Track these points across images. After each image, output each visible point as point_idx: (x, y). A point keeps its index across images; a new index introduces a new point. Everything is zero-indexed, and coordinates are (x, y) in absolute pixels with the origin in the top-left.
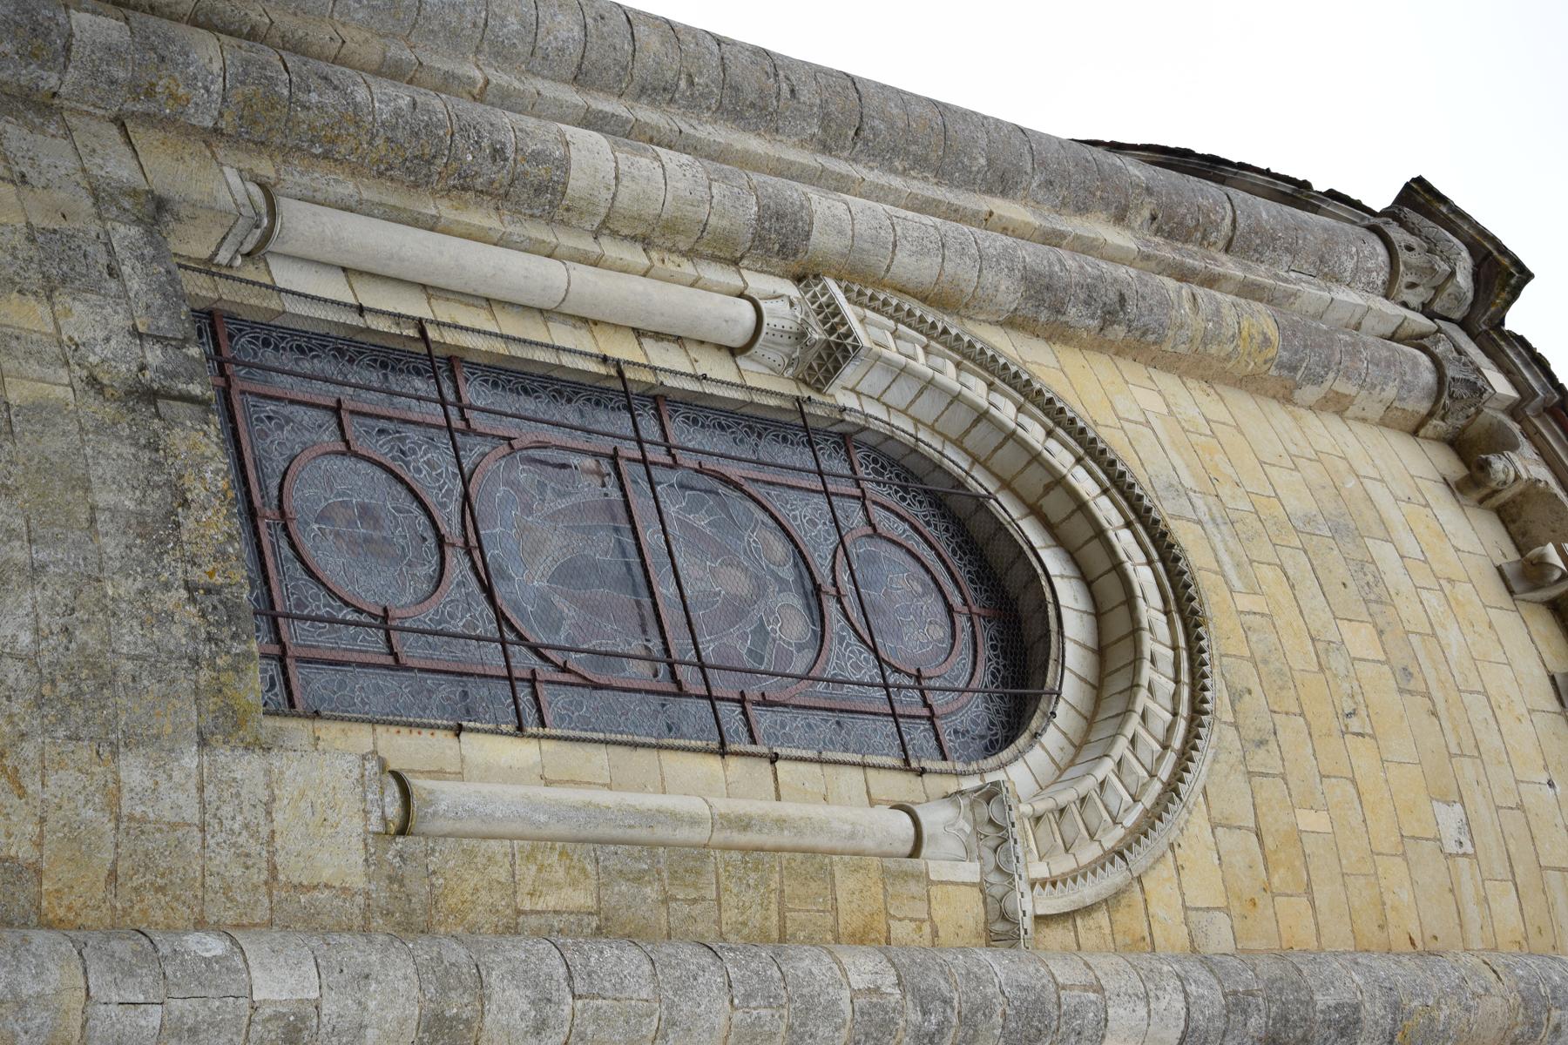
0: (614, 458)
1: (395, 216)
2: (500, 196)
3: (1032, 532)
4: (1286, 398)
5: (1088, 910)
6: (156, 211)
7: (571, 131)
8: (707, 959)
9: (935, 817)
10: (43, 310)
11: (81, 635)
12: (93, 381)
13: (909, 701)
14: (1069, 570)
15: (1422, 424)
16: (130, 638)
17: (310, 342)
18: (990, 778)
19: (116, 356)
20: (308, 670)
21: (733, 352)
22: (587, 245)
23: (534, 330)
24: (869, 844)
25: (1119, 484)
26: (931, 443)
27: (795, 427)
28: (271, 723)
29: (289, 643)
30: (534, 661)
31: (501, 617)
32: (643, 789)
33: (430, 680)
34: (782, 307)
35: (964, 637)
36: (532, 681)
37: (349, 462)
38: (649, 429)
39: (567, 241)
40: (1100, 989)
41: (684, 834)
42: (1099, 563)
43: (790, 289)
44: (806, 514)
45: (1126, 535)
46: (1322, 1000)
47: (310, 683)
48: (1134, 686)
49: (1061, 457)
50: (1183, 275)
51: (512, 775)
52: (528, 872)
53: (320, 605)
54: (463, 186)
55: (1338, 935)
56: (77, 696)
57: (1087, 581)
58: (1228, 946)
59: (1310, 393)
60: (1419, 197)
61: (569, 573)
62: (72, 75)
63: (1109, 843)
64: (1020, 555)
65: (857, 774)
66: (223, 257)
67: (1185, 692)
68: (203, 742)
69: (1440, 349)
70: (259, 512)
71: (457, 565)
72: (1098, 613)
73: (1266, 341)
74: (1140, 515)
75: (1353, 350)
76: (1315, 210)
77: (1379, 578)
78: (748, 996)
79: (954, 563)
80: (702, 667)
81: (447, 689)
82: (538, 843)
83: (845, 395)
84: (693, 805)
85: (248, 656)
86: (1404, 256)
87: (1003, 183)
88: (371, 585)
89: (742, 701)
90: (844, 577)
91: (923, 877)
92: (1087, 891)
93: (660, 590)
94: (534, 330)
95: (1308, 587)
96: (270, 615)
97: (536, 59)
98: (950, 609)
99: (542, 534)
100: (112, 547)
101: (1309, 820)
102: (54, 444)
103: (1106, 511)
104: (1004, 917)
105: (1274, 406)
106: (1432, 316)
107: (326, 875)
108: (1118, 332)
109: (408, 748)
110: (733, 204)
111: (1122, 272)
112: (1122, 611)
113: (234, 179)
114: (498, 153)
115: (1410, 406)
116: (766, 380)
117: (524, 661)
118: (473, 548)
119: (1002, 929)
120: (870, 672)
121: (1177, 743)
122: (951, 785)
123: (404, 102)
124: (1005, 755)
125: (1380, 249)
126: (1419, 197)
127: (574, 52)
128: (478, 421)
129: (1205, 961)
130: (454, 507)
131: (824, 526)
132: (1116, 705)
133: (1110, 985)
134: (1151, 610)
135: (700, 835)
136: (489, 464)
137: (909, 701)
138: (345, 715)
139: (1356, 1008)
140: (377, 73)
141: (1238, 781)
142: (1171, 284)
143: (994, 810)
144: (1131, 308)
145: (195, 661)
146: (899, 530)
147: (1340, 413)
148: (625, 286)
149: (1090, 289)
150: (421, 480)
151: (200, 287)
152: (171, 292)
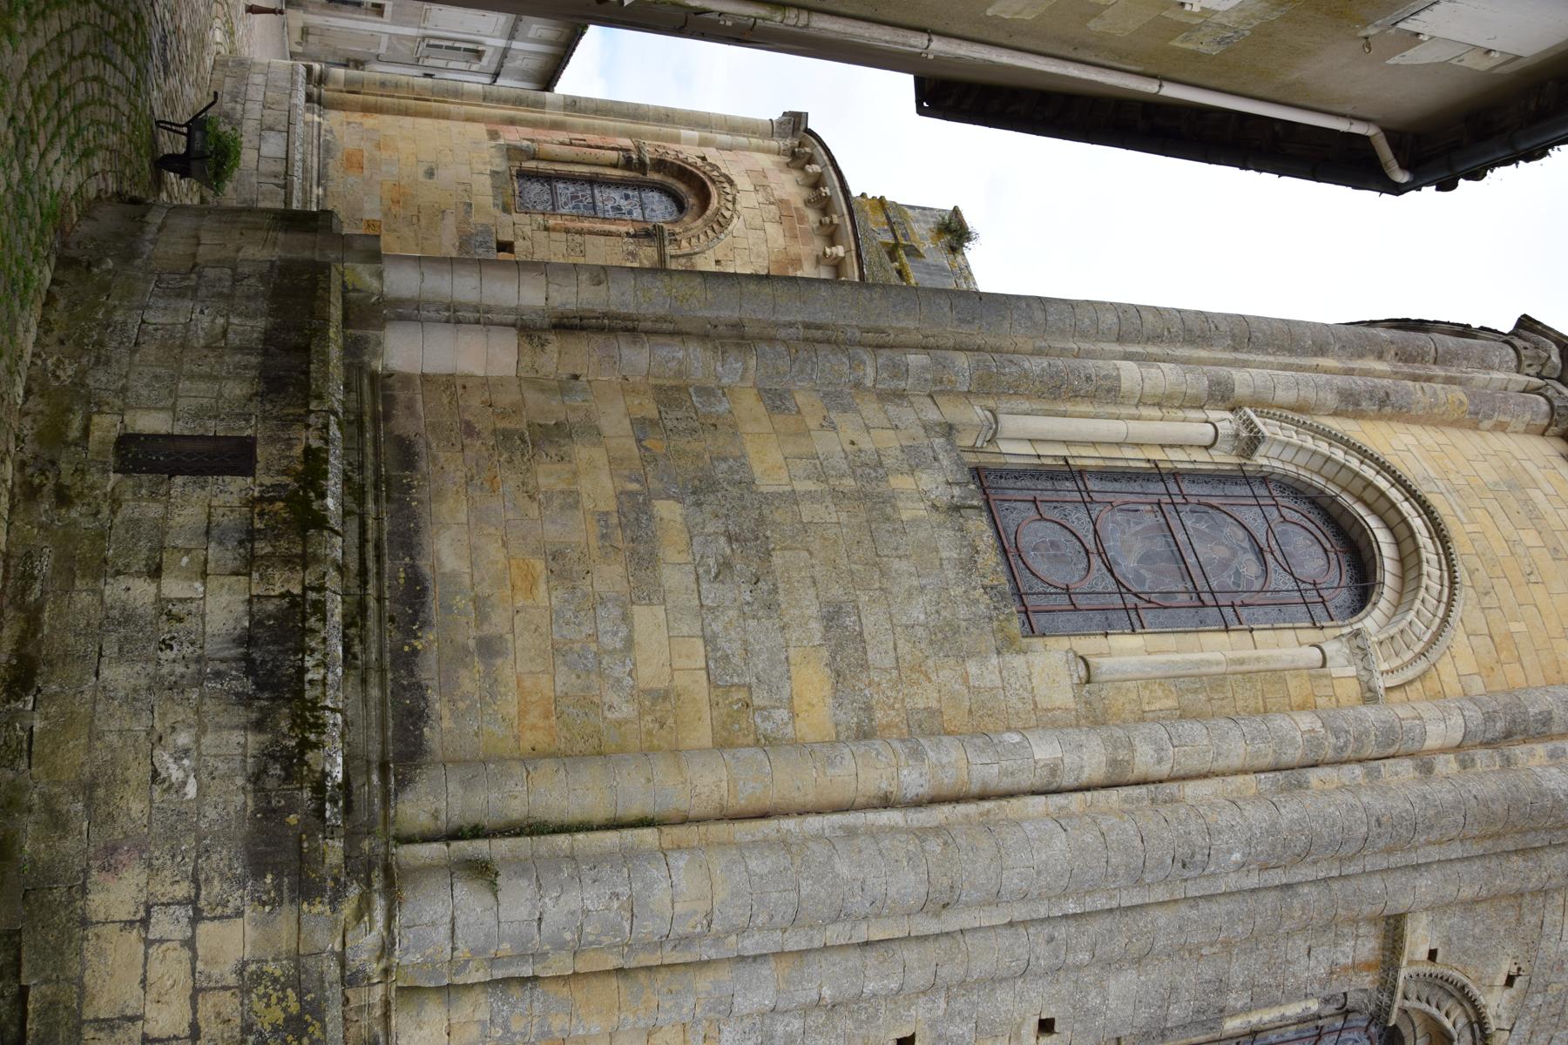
0: (1159, 504)
1: (1048, 413)
2: (1091, 397)
3: (1360, 509)
4: (1475, 427)
5: (1410, 682)
6: (949, 430)
7: (1118, 363)
8: (1232, 724)
9: (1331, 648)
10: (911, 480)
11: (944, 613)
12: (934, 506)
13: (1312, 596)
14: (1381, 525)
15: (1546, 430)
16: (963, 612)
17: (1019, 474)
18: (1356, 627)
19: (942, 494)
20: (1040, 616)
21: (1207, 448)
22: (1133, 411)
23: (1116, 453)
24: (1301, 664)
25: (1399, 481)
26: (1305, 475)
27: (1241, 477)
28: (1025, 641)
29: (1030, 607)
30: (1136, 600)
31: (1118, 582)
32: (1192, 651)
33: (1091, 614)
34: (1226, 424)
35: (1334, 562)
36: (1136, 609)
37: (1043, 523)
38: (1173, 488)
39: (1124, 411)
40: (1421, 718)
41: (1214, 669)
42: (1395, 519)
43: (1229, 415)
44: (1251, 516)
45: (1406, 504)
46: (1532, 711)
47: (1039, 621)
48: (1420, 575)
49: (1369, 472)
50: (1415, 378)
51: (1133, 652)
52: (1146, 694)
53: (1039, 587)
54: (1076, 395)
55: (1537, 678)
56: (945, 638)
57: (1390, 529)
58: (1483, 691)
59: (1487, 424)
60: (1526, 324)
61: (1146, 558)
62: (910, 381)
63: (1417, 649)
64: (1356, 521)
65: (1291, 633)
66: (979, 444)
67: (1446, 575)
68: (999, 653)
69: (1549, 394)
70: (1008, 550)
71: (1096, 561)
72: (1398, 543)
73: (1461, 403)
74: (1412, 494)
75: (1505, 400)
76: (1475, 337)
77: (1535, 507)
78: (1253, 739)
79: (1324, 529)
80: (1212, 593)
81: (1098, 616)
82: (1148, 681)
83: (1262, 459)
84: (1218, 656)
85: (1012, 614)
86: (1523, 352)
87: (1321, 350)
88: (1057, 576)
89: (1233, 605)
90: (1273, 543)
91: (1328, 676)
92: (1410, 673)
93: (1188, 560)
94: (1116, 453)
95: (1500, 516)
96: (1020, 596)
97: (1100, 335)
98: (1326, 551)
99: (1131, 541)
100: (951, 574)
101: (1515, 627)
102: (922, 535)
103: (1395, 495)
104: (1370, 690)
105: (1470, 432)
106: (1542, 378)
107: (1058, 704)
108: (1388, 410)
109: (1085, 645)
110: (1197, 382)
111: (1386, 382)
112: (1410, 541)
113: (979, 410)
114: (1088, 379)
115: (1538, 422)
116: (1224, 458)
117: (1131, 600)
118: (1102, 553)
119: (1370, 696)
120: (1291, 585)
121: (1445, 599)
122: (1337, 632)
123: (1045, 365)
124: (1361, 615)
125: (1511, 351)
126: (1526, 324)
127: (1116, 328)
128: (1096, 497)
129: (1471, 699)
130: (1091, 536)
131: (1260, 520)
132: (1413, 585)
133: (1425, 716)
134: (1423, 538)
135: (1222, 669)
136: (1103, 515)
137: (1312, 596)
138: (1056, 634)
139: (1550, 713)
140: (1032, 354)
141: (1477, 613)
142: (1410, 383)
143: (1359, 642)
144: (1393, 398)
145: (991, 619)
146: (1296, 517)
147: (1504, 431)
148: (1154, 426)
149: (1371, 392)
150: (1074, 526)
151: (971, 459)
152: (959, 463)
